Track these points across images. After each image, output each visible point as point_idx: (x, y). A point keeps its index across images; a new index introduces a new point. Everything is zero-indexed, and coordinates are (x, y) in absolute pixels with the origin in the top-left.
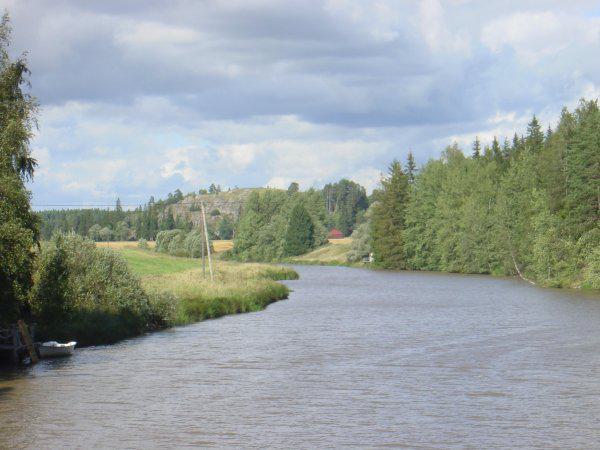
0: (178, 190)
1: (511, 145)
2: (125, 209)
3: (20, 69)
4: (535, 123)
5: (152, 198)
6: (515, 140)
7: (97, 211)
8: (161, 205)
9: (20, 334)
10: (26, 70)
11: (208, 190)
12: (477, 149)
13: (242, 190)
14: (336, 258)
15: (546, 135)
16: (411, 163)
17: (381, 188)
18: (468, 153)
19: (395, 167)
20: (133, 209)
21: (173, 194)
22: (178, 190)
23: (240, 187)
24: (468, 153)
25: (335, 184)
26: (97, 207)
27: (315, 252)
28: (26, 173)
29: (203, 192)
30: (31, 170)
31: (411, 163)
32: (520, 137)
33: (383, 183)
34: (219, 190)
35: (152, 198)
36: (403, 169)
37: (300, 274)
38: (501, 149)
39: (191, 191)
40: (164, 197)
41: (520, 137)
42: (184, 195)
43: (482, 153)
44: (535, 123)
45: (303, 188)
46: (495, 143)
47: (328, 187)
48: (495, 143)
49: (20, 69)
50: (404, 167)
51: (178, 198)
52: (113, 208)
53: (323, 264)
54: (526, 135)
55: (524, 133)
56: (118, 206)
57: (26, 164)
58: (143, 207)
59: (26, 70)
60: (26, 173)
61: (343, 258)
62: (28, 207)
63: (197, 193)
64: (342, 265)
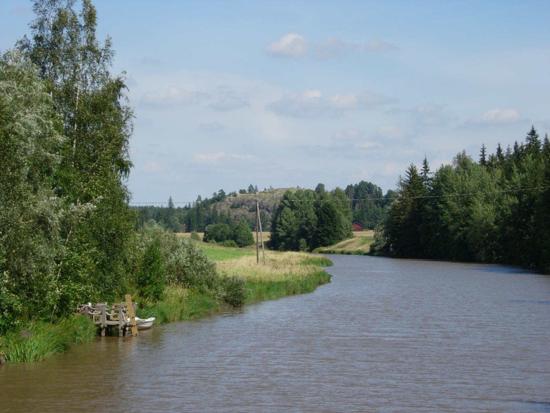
0: (222, 190)
1: (512, 151)
2: (176, 206)
3: (119, 85)
4: (533, 132)
5: (199, 197)
6: (516, 147)
7: (152, 208)
8: (206, 204)
9: (78, 235)
10: (124, 86)
11: (247, 189)
12: (483, 155)
13: (277, 190)
14: (360, 248)
15: (543, 143)
16: (426, 167)
17: (326, 191)
18: (476, 159)
19: (413, 171)
20: (182, 206)
21: (218, 193)
22: (222, 190)
23: (275, 187)
24: (476, 159)
25: (356, 185)
26: (151, 205)
27: (342, 243)
28: (123, 173)
29: (242, 192)
30: (127, 170)
31: (426, 167)
32: (520, 145)
33: (401, 183)
34: (256, 190)
35: (199, 197)
36: (419, 172)
37: (334, 262)
38: (505, 155)
39: (232, 191)
40: (210, 197)
41: (520, 145)
42: (227, 194)
43: (487, 159)
44: (533, 132)
45: (329, 188)
46: (499, 150)
47: (350, 187)
48: (499, 150)
49: (119, 85)
50: (419, 170)
51: (220, 198)
52: (166, 206)
53: (349, 253)
54: (525, 143)
55: (523, 141)
56: (170, 203)
57: (124, 167)
58: (191, 205)
59: (124, 86)
60: (123, 173)
61: (366, 248)
62: (162, 209)
63: (238, 193)
64: (366, 254)
